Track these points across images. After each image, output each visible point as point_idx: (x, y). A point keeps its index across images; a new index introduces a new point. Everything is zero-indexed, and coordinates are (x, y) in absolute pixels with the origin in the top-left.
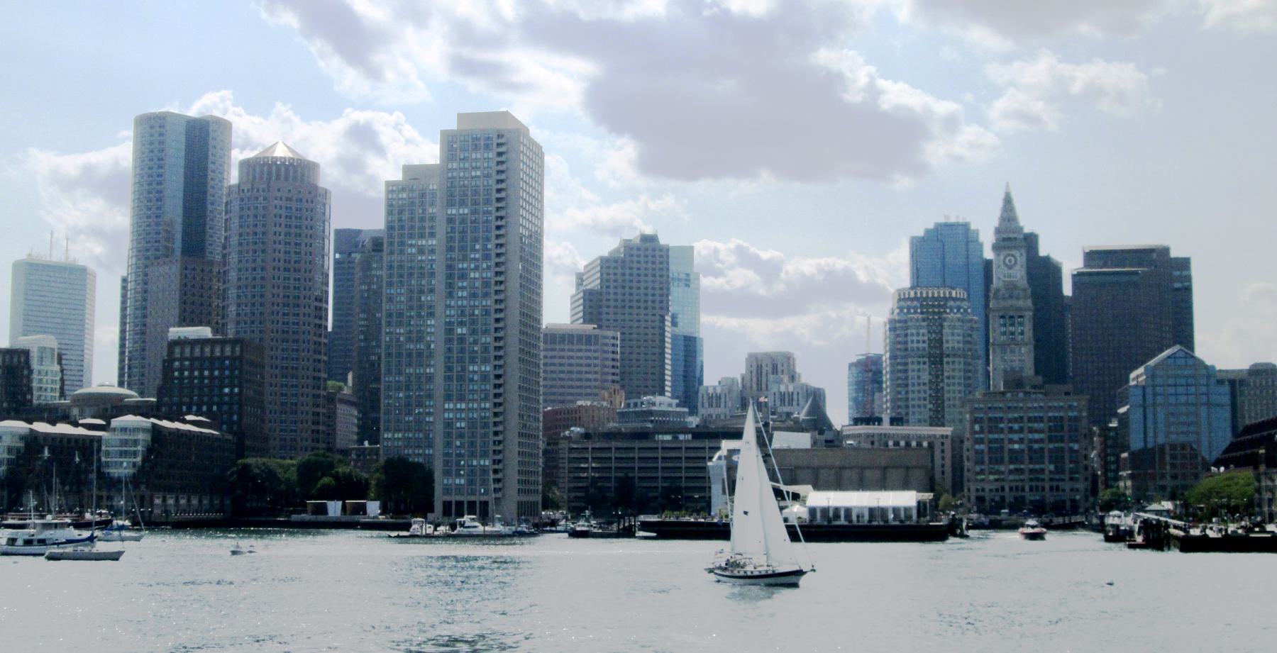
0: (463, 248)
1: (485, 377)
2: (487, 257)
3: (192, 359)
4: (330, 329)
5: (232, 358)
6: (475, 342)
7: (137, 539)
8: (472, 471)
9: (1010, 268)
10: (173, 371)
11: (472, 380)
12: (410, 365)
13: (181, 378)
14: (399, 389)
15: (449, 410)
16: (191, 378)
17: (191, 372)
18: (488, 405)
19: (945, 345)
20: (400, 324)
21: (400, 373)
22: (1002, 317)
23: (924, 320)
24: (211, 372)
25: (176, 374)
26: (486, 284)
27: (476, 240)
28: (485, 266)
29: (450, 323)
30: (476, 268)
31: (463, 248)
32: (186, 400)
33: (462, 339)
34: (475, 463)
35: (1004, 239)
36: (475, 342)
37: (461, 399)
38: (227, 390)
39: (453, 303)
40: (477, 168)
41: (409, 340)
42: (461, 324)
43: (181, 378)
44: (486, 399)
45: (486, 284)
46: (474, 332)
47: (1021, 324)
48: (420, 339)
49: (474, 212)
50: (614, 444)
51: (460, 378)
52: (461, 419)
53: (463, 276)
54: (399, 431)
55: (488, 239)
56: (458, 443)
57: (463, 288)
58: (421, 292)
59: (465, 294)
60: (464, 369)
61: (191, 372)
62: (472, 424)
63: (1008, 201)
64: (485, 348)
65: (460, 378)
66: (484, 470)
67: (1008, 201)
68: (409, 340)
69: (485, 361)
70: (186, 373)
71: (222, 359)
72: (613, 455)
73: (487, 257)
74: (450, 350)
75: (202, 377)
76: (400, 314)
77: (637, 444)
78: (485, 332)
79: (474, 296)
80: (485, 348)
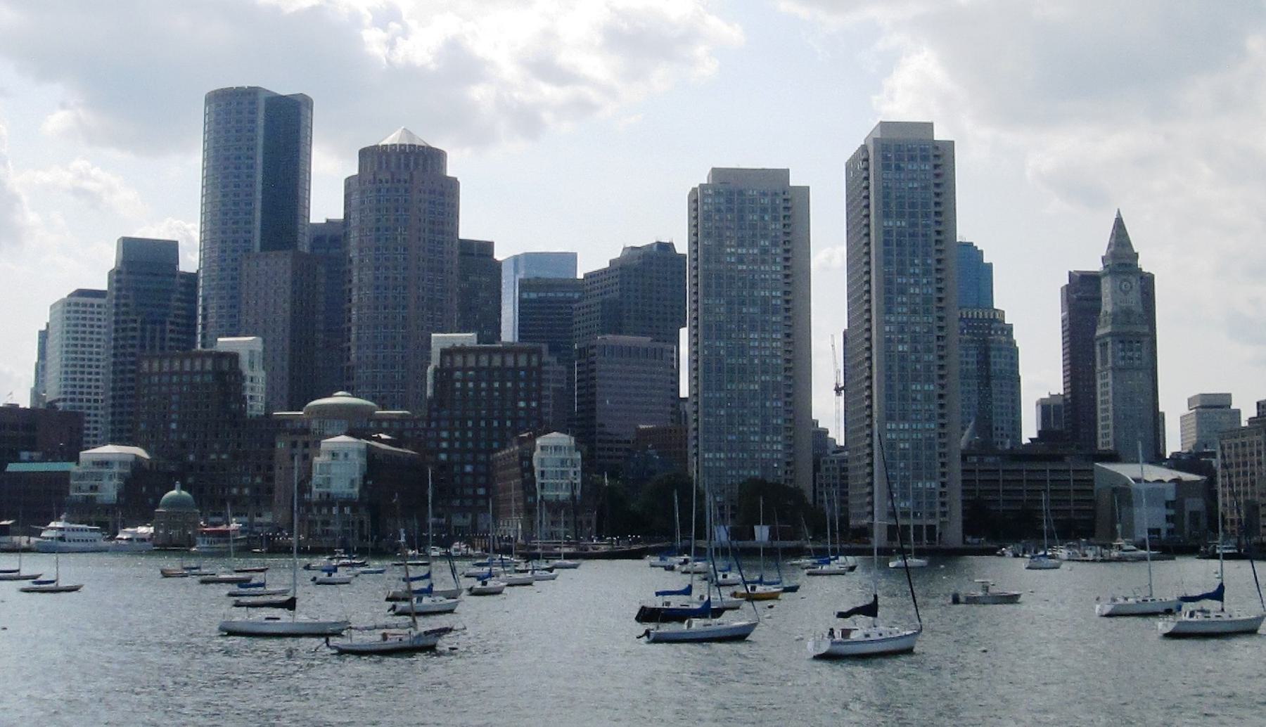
0: (902, 263)
1: (928, 397)
2: (926, 273)
3: (478, 369)
4: (12, 467)
5: (529, 369)
6: (918, 361)
7: (575, 567)
8: (918, 494)
9: (1126, 293)
10: (454, 381)
11: (914, 399)
12: (731, 381)
13: (464, 389)
14: (720, 406)
15: (891, 430)
16: (477, 390)
17: (490, 383)
18: (932, 426)
19: (993, 368)
20: (719, 338)
21: (720, 389)
22: (1122, 342)
23: (973, 341)
24: (503, 383)
25: (458, 385)
26: (927, 300)
27: (914, 254)
28: (925, 281)
29: (889, 340)
30: (916, 284)
31: (902, 263)
32: (472, 414)
33: (903, 357)
34: (920, 485)
35: (1120, 265)
36: (918, 361)
37: (904, 418)
38: (522, 404)
39: (893, 319)
40: (913, 179)
41: (730, 354)
42: (901, 341)
43: (464, 389)
44: (929, 420)
45: (927, 300)
46: (915, 350)
47: (1139, 350)
48: (742, 353)
49: (914, 225)
50: (1026, 466)
51: (903, 398)
52: (904, 440)
53: (902, 292)
54: (720, 450)
55: (927, 254)
56: (902, 465)
57: (903, 303)
58: (743, 303)
59: (905, 310)
60: (905, 388)
61: (490, 383)
62: (916, 445)
63: (1119, 225)
64: (928, 367)
65: (903, 398)
66: (931, 492)
67: (1119, 225)
68: (730, 354)
69: (929, 380)
70: (471, 385)
71: (516, 369)
72: (1025, 476)
73: (926, 273)
74: (890, 368)
75: (490, 389)
76: (719, 328)
77: (1049, 466)
78: (929, 351)
79: (915, 312)
80: (928, 367)
